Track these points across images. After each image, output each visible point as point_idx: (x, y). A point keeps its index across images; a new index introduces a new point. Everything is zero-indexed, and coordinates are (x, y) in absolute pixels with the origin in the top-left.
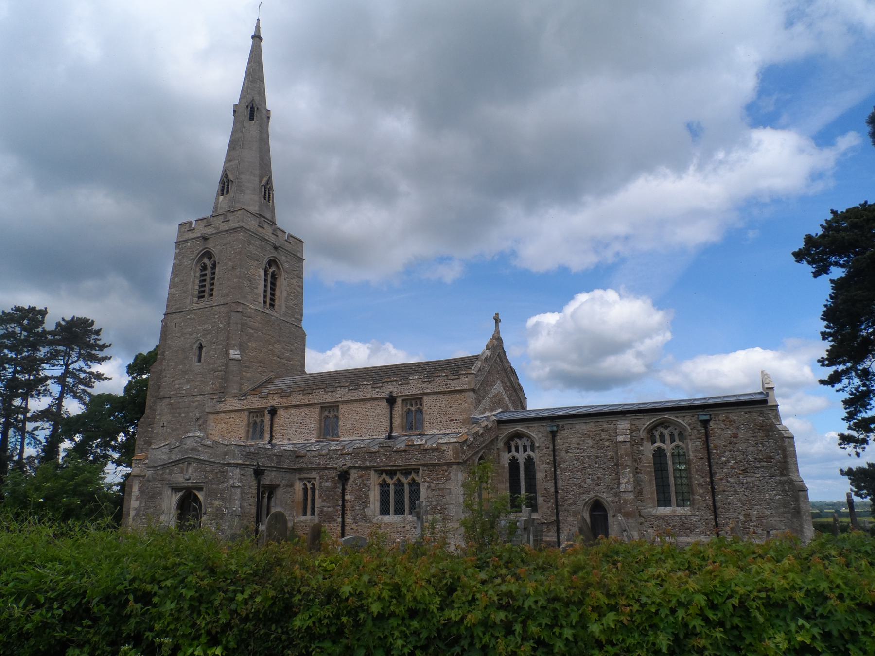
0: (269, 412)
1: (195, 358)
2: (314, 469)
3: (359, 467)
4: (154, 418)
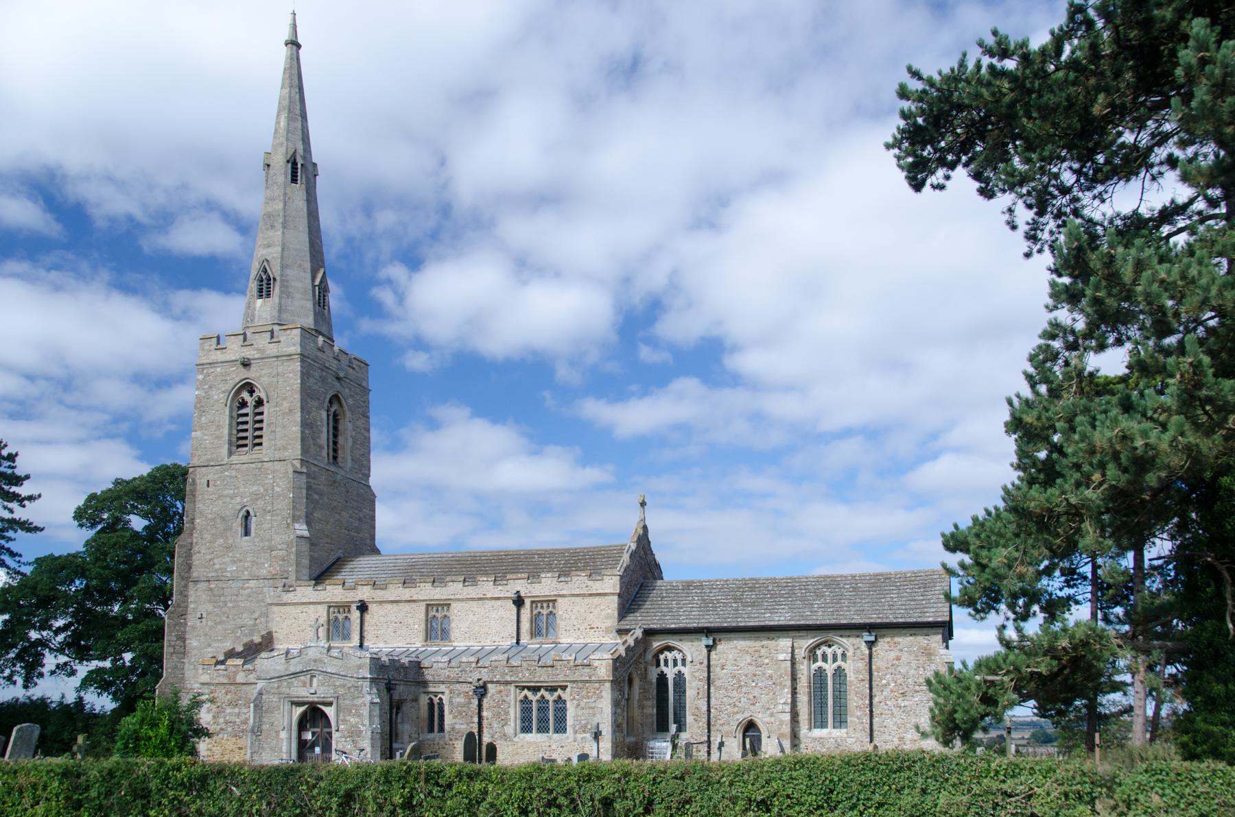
0: (358, 608)
1: (240, 530)
2: (443, 682)
3: (498, 682)
4: (187, 607)
